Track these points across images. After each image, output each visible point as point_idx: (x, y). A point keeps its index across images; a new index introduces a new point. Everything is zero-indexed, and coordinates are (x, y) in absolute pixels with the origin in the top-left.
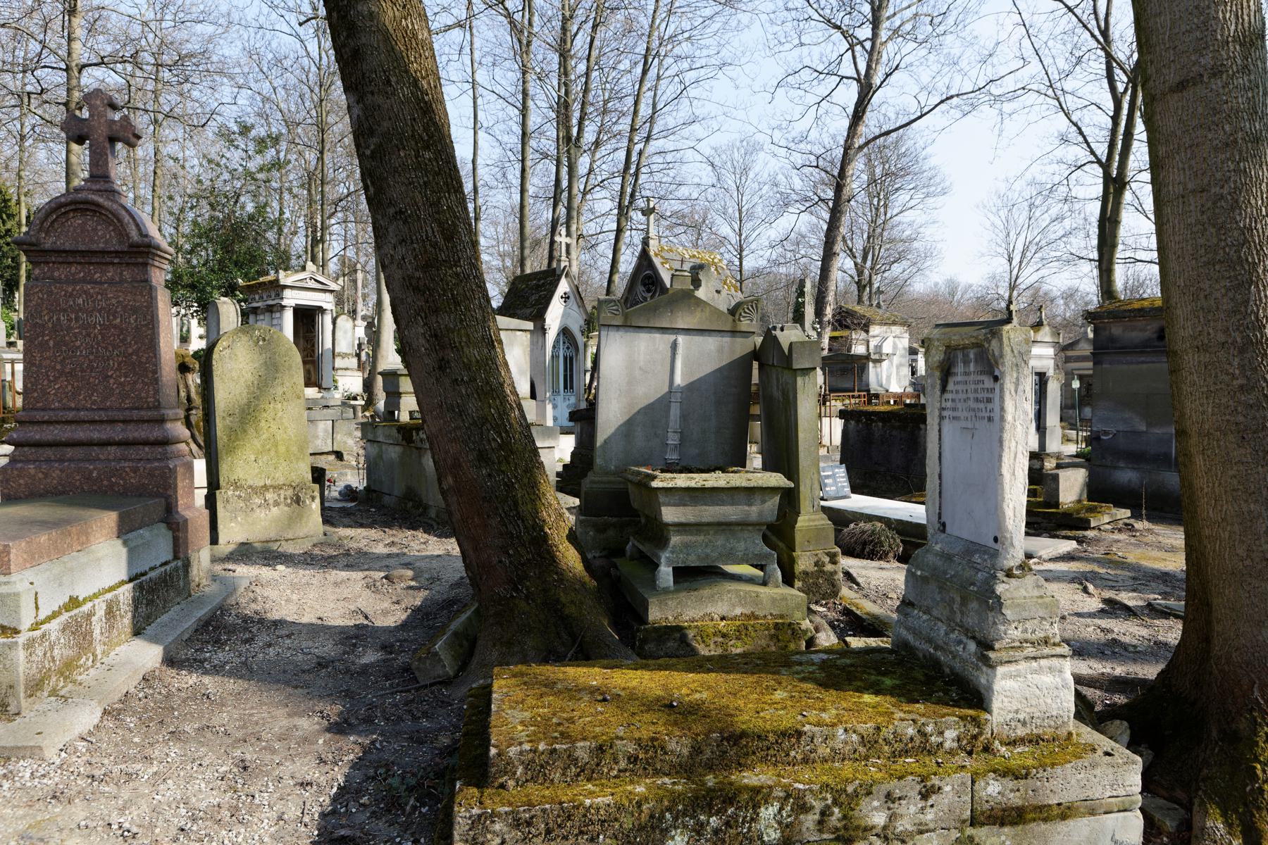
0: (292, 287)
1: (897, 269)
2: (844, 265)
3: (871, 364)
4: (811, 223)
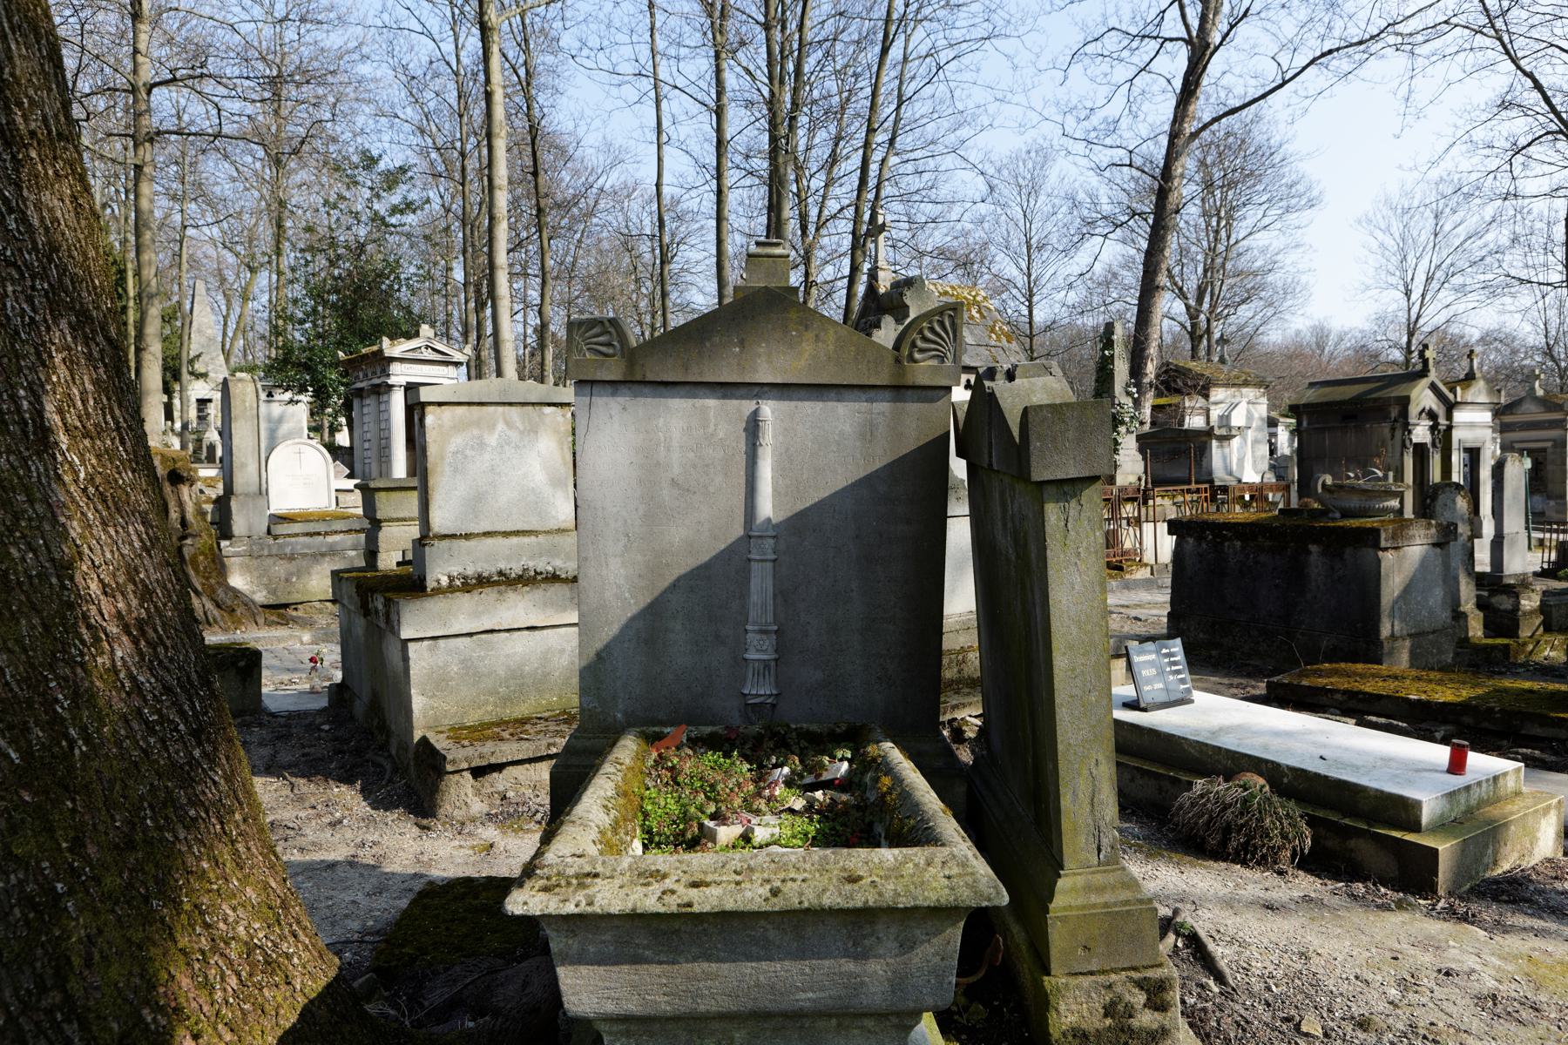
0: (401, 360)
1: (1245, 312)
2: (1170, 310)
3: (1214, 443)
4: (1117, 253)
